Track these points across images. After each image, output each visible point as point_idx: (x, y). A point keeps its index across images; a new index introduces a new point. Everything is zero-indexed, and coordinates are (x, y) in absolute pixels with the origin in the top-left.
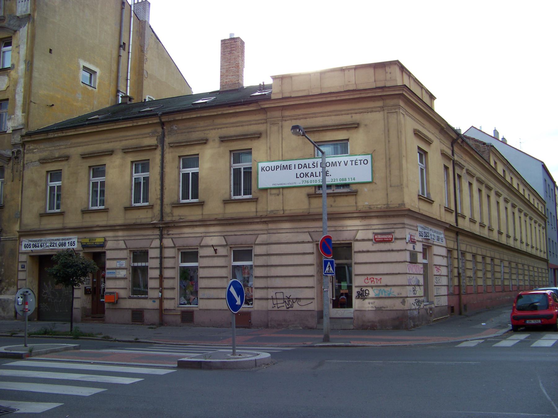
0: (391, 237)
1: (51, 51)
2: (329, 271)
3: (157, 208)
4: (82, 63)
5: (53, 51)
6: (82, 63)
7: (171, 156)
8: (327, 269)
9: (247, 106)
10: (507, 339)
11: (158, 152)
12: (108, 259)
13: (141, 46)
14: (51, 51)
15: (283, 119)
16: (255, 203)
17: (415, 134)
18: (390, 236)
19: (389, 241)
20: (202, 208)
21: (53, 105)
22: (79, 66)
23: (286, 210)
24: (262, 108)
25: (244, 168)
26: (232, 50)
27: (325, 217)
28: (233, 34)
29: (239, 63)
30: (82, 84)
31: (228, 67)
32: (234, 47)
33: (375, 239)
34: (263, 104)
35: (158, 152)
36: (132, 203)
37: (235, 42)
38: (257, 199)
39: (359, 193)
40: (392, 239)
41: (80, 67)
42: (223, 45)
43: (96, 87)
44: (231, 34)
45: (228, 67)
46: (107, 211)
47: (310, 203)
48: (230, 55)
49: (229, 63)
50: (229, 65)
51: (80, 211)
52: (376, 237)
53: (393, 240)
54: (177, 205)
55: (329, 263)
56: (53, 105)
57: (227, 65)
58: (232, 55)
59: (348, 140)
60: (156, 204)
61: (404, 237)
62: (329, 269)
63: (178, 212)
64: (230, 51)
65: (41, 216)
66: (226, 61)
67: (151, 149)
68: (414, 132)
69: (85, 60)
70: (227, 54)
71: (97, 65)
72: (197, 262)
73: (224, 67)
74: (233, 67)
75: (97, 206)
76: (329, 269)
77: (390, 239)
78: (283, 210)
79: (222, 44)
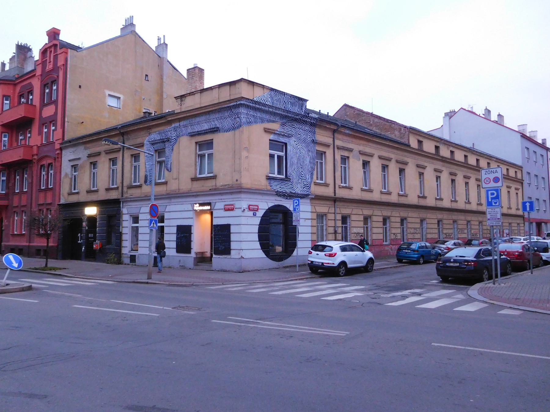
1: (80, 87)
2: (153, 226)
3: (120, 189)
4: (107, 92)
5: (82, 87)
6: (107, 92)
7: (127, 154)
8: (152, 225)
10: (461, 299)
11: (121, 152)
13: (161, 75)
14: (80, 87)
15: (262, 121)
18: (233, 207)
19: (232, 210)
21: (83, 122)
22: (105, 95)
23: (181, 189)
26: (193, 77)
28: (197, 64)
29: (196, 86)
30: (108, 107)
32: (193, 74)
33: (225, 208)
34: (169, 118)
35: (121, 152)
36: (110, 186)
37: (195, 70)
38: (167, 182)
41: (106, 95)
42: (188, 73)
43: (121, 108)
44: (194, 64)
46: (98, 191)
50: (191, 87)
51: (527, 197)
52: (225, 207)
53: (235, 209)
54: (130, 187)
55: (154, 221)
56: (83, 122)
57: (190, 88)
60: (120, 187)
62: (153, 225)
63: (131, 191)
64: (192, 77)
65: (69, 195)
67: (118, 151)
69: (110, 90)
71: (121, 93)
72: (138, 223)
74: (193, 89)
76: (153, 225)
79: (187, 73)
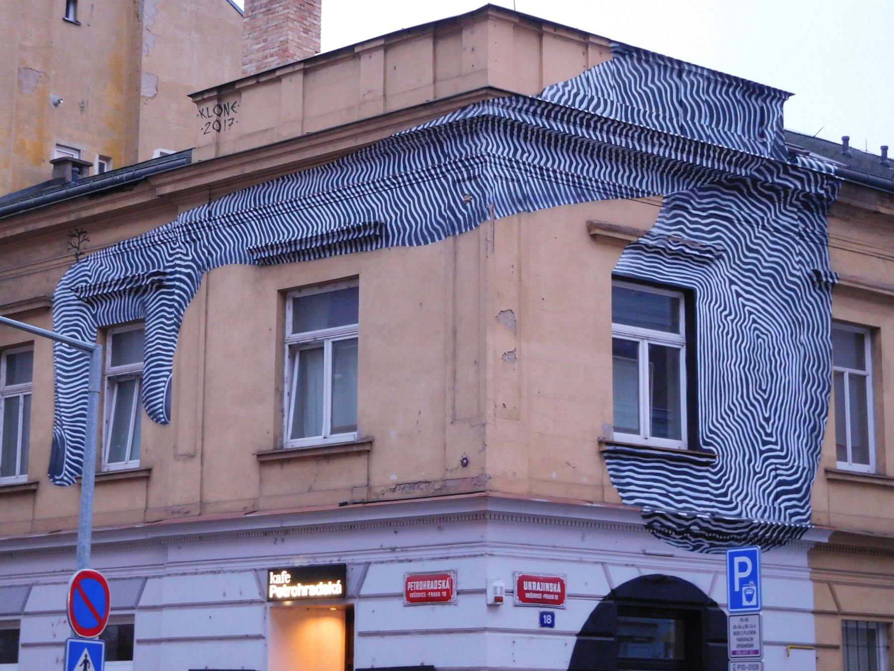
0: (448, 587)
9: (129, 193)
12: (25, 645)
16: (144, 483)
17: (594, 237)
18: (445, 585)
19: (444, 598)
20: (34, 500)
24: (162, 196)
25: (333, 342)
27: (85, 542)
31: (261, 54)
33: (408, 592)
38: (149, 470)
39: (377, 444)
40: (449, 592)
45: (261, 54)
47: (261, 481)
48: (266, 18)
49: (262, 44)
50: (264, 49)
53: (454, 595)
58: (271, 16)
59: (356, 277)
61: (481, 586)
66: (257, 38)
68: (589, 230)
70: (260, 16)
73: (252, 57)
74: (272, 55)
75: (864, 377)
77: (444, 594)
78: (201, 502)
